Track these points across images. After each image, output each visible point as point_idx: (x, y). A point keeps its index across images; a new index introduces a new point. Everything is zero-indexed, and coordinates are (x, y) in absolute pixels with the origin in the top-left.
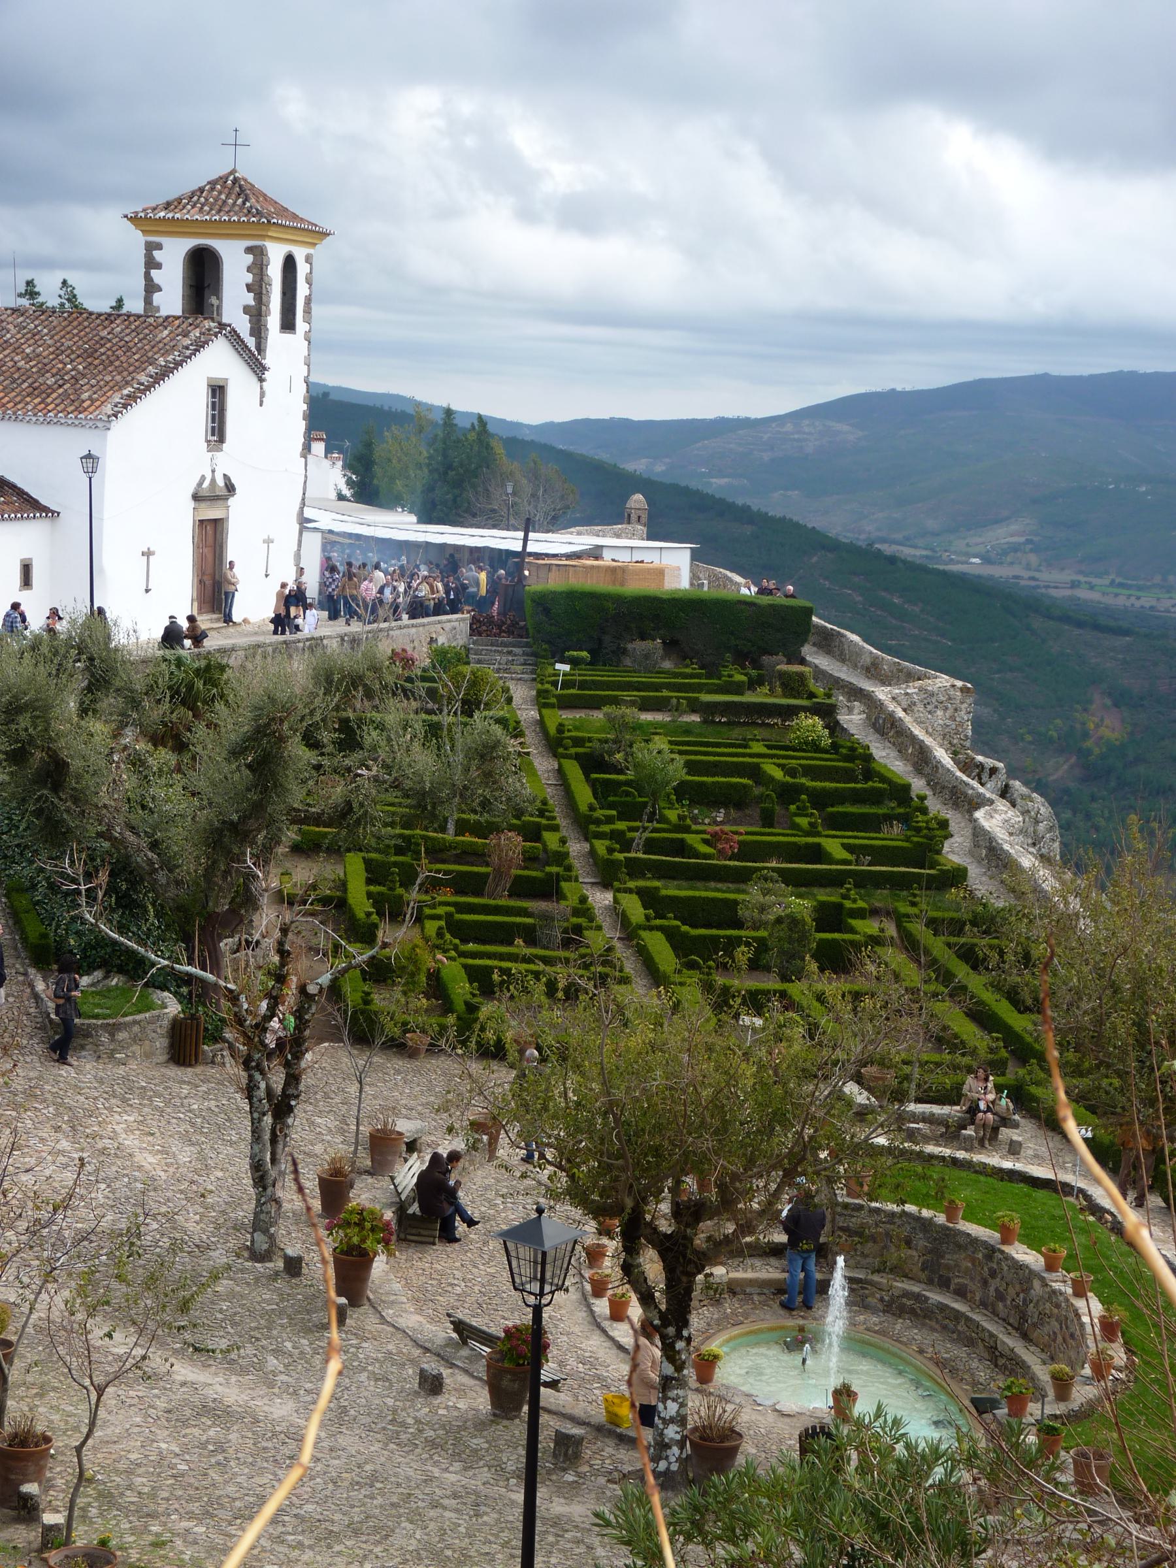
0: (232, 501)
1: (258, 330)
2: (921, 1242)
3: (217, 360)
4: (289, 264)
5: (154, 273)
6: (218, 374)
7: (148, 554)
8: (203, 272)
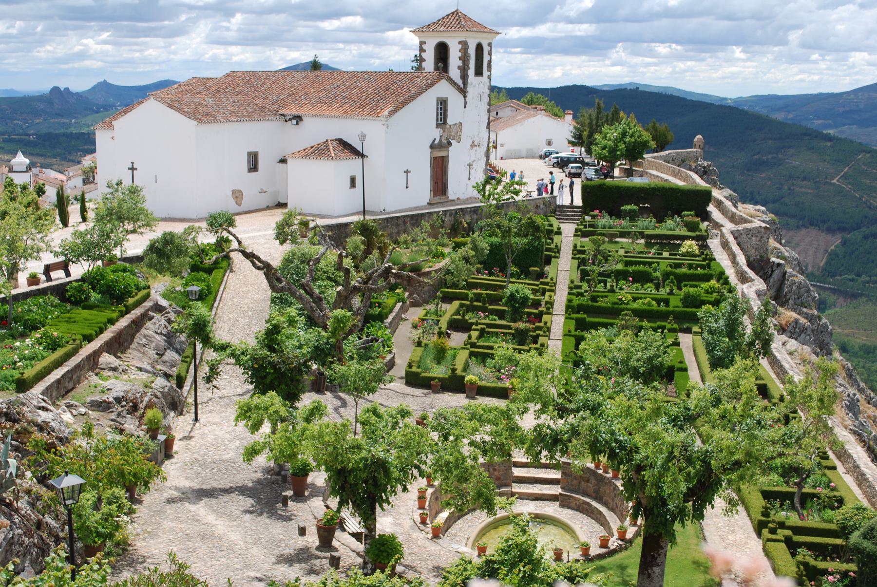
0: (450, 149)
1: (464, 77)
2: (593, 481)
3: (443, 89)
4: (479, 48)
5: (423, 54)
6: (443, 95)
7: (407, 172)
8: (442, 51)
